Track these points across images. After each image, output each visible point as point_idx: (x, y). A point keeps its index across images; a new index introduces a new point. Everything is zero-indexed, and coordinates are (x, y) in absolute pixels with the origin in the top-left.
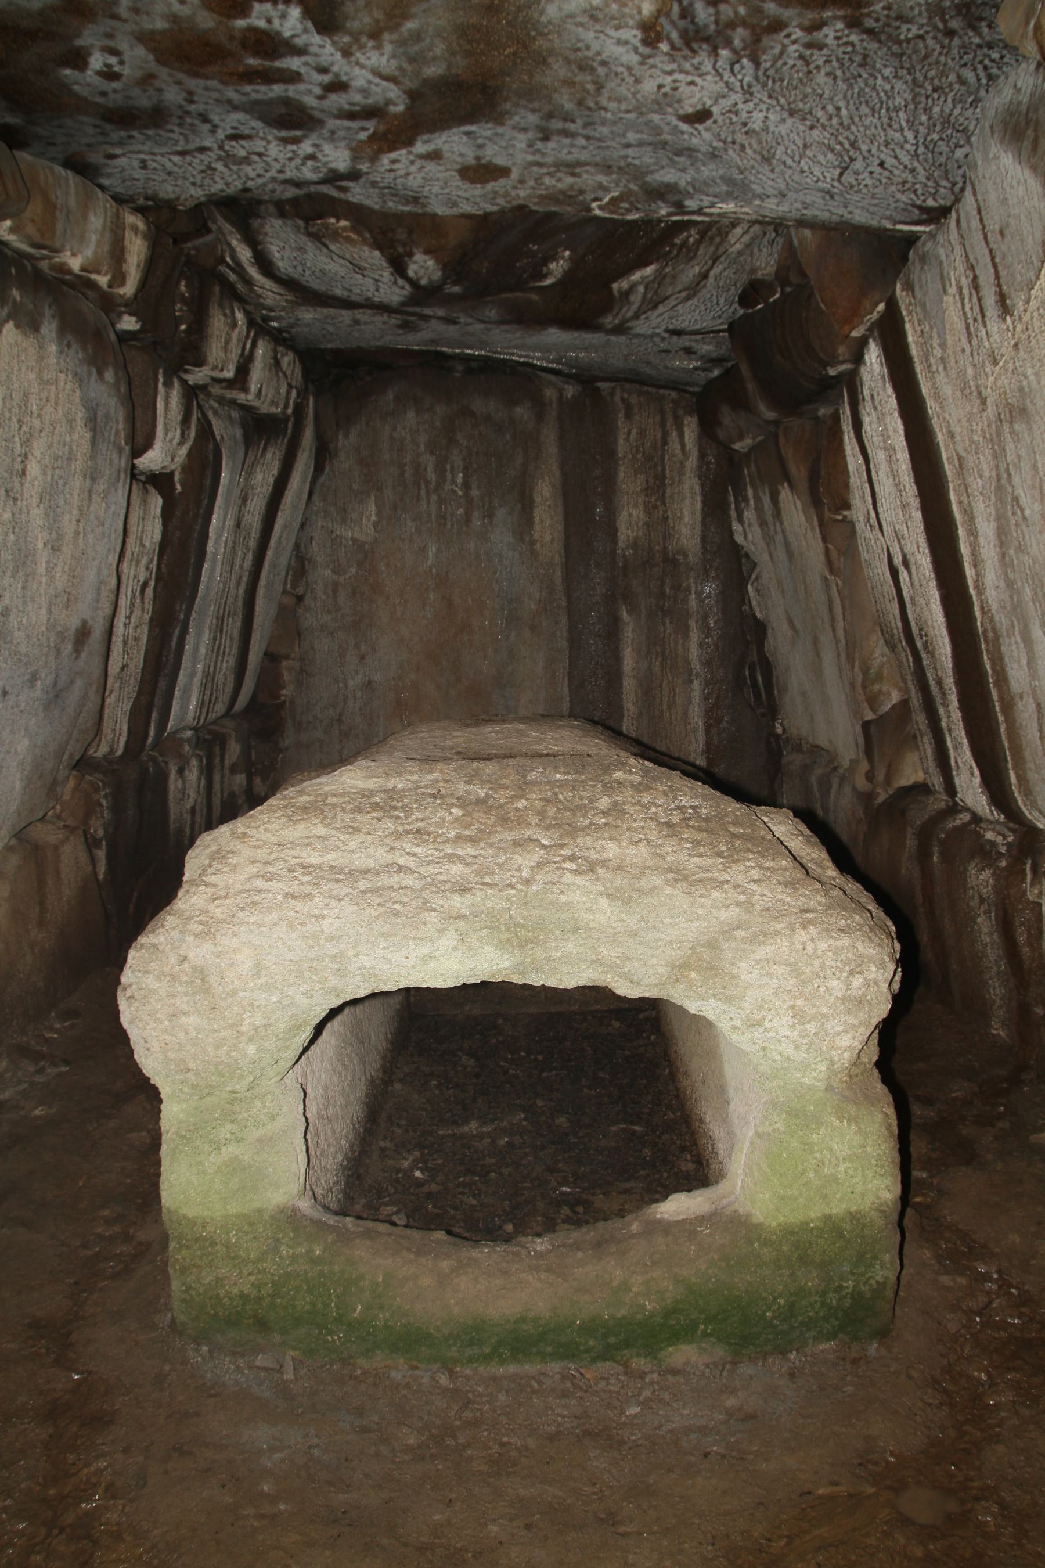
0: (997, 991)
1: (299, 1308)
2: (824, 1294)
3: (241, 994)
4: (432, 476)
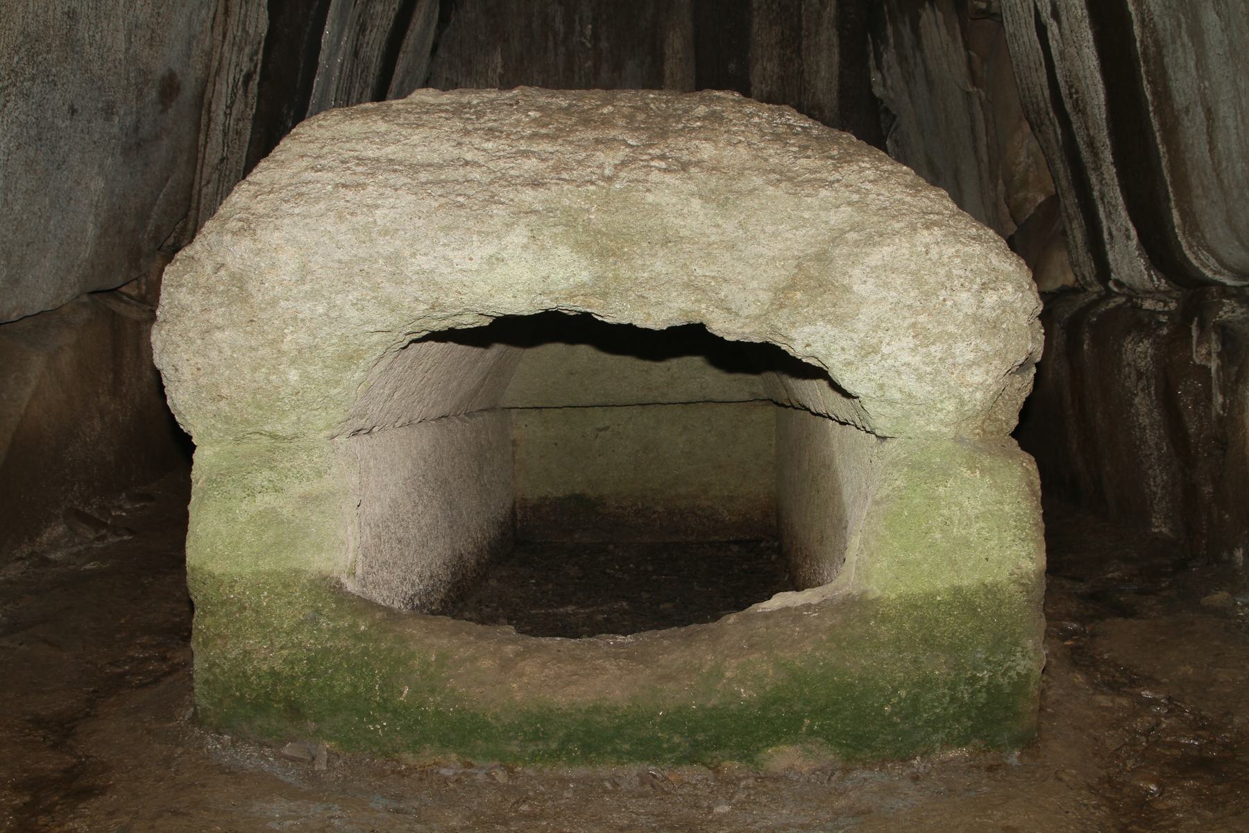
0: (1158, 480)
1: (337, 690)
2: (953, 687)
3: (282, 303)
4: (559, 26)
